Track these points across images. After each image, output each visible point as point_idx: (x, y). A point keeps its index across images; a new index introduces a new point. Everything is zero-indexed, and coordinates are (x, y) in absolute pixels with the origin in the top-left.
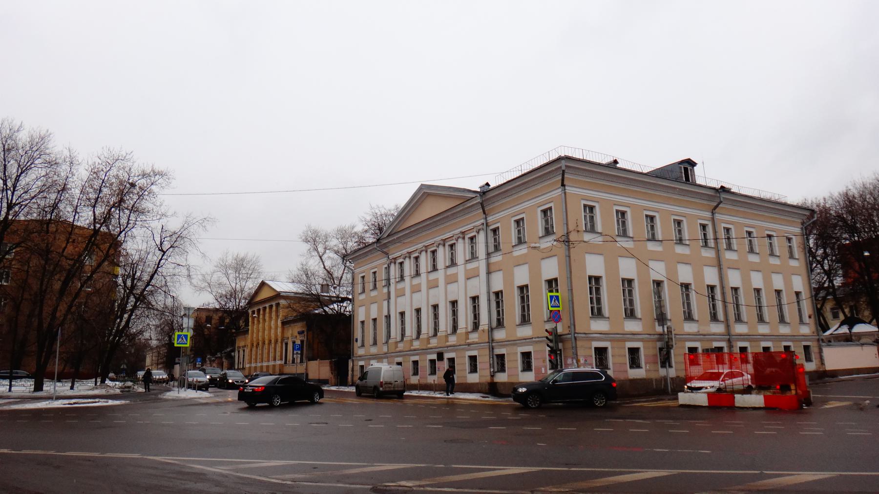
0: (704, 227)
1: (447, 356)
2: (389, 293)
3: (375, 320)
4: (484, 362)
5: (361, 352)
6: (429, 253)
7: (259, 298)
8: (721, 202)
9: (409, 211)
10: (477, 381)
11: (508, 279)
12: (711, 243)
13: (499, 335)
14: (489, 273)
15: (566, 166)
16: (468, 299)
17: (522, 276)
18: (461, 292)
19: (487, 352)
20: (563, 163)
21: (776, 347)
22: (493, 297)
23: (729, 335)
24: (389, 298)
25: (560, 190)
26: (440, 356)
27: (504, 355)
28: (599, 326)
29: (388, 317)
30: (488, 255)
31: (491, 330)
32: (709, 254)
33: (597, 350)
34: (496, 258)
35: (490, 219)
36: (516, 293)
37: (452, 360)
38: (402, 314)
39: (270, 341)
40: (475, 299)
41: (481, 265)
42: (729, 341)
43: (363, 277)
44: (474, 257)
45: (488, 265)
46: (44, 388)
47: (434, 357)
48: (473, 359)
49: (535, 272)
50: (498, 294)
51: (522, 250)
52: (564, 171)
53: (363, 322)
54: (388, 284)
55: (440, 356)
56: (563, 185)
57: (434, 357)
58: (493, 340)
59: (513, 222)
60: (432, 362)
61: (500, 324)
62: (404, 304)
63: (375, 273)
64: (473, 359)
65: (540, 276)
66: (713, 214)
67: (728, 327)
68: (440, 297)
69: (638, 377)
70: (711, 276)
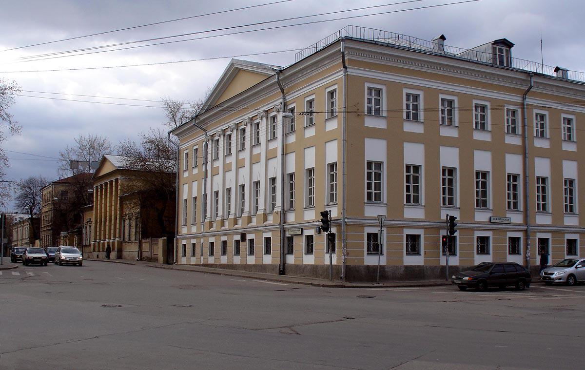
0: (514, 113)
1: (249, 237)
2: (206, 170)
3: (310, 171)
4: (276, 245)
5: (184, 231)
6: (239, 131)
7: (102, 173)
8: (531, 87)
9: (248, 97)
12: (519, 130)
15: (346, 48)
19: (278, 234)
20: (341, 47)
21: (133, 210)
22: (287, 179)
23: (527, 225)
24: (206, 177)
25: (342, 72)
26: (243, 237)
28: (481, 216)
29: (206, 195)
31: (284, 213)
32: (514, 141)
34: (292, 139)
35: (289, 98)
36: (305, 174)
37: (252, 241)
40: (273, 180)
42: (526, 232)
43: (187, 154)
46: (530, 286)
48: (268, 240)
49: (321, 155)
50: (291, 176)
52: (343, 53)
53: (186, 200)
55: (243, 237)
56: (345, 67)
58: (285, 222)
60: (237, 242)
62: (218, 183)
64: (268, 240)
65: (505, 172)
67: (526, 217)
70: (513, 164)
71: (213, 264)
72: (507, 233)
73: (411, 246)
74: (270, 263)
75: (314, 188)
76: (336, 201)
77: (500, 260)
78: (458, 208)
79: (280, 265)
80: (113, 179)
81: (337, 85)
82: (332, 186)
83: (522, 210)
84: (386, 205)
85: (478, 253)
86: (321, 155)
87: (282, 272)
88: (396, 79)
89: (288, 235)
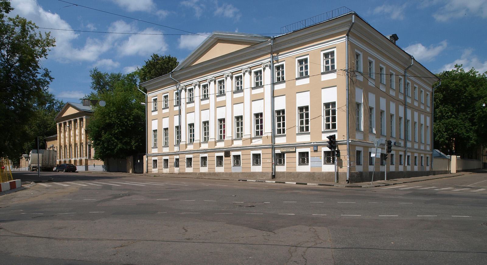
1: (233, 154)
2: (180, 110)
3: (166, 129)
6: (253, 73)
10: (223, 171)
11: (291, 101)
13: (280, 141)
14: (273, 97)
16: (253, 115)
17: (303, 100)
18: (247, 111)
27: (240, 156)
29: (178, 128)
30: (273, 84)
31: (274, 137)
33: (154, 160)
38: (191, 125)
39: (70, 145)
41: (267, 90)
44: (258, 85)
45: (273, 92)
47: (222, 154)
51: (167, 111)
53: (155, 131)
54: (179, 104)
57: (222, 154)
59: (175, 94)
61: (281, 132)
63: (166, 97)
66: (405, 72)
68: (211, 116)
69: (456, 165)
71: (223, 173)
72: (400, 152)
73: (305, 162)
74: (261, 171)
75: (168, 137)
76: (168, 144)
77: (228, 171)
78: (394, 138)
79: (272, 172)
80: (62, 122)
81: (285, 62)
82: (155, 140)
83: (403, 138)
84: (362, 132)
85: (325, 163)
86: (160, 124)
87: (274, 177)
88: (369, 51)
89: (278, 151)
